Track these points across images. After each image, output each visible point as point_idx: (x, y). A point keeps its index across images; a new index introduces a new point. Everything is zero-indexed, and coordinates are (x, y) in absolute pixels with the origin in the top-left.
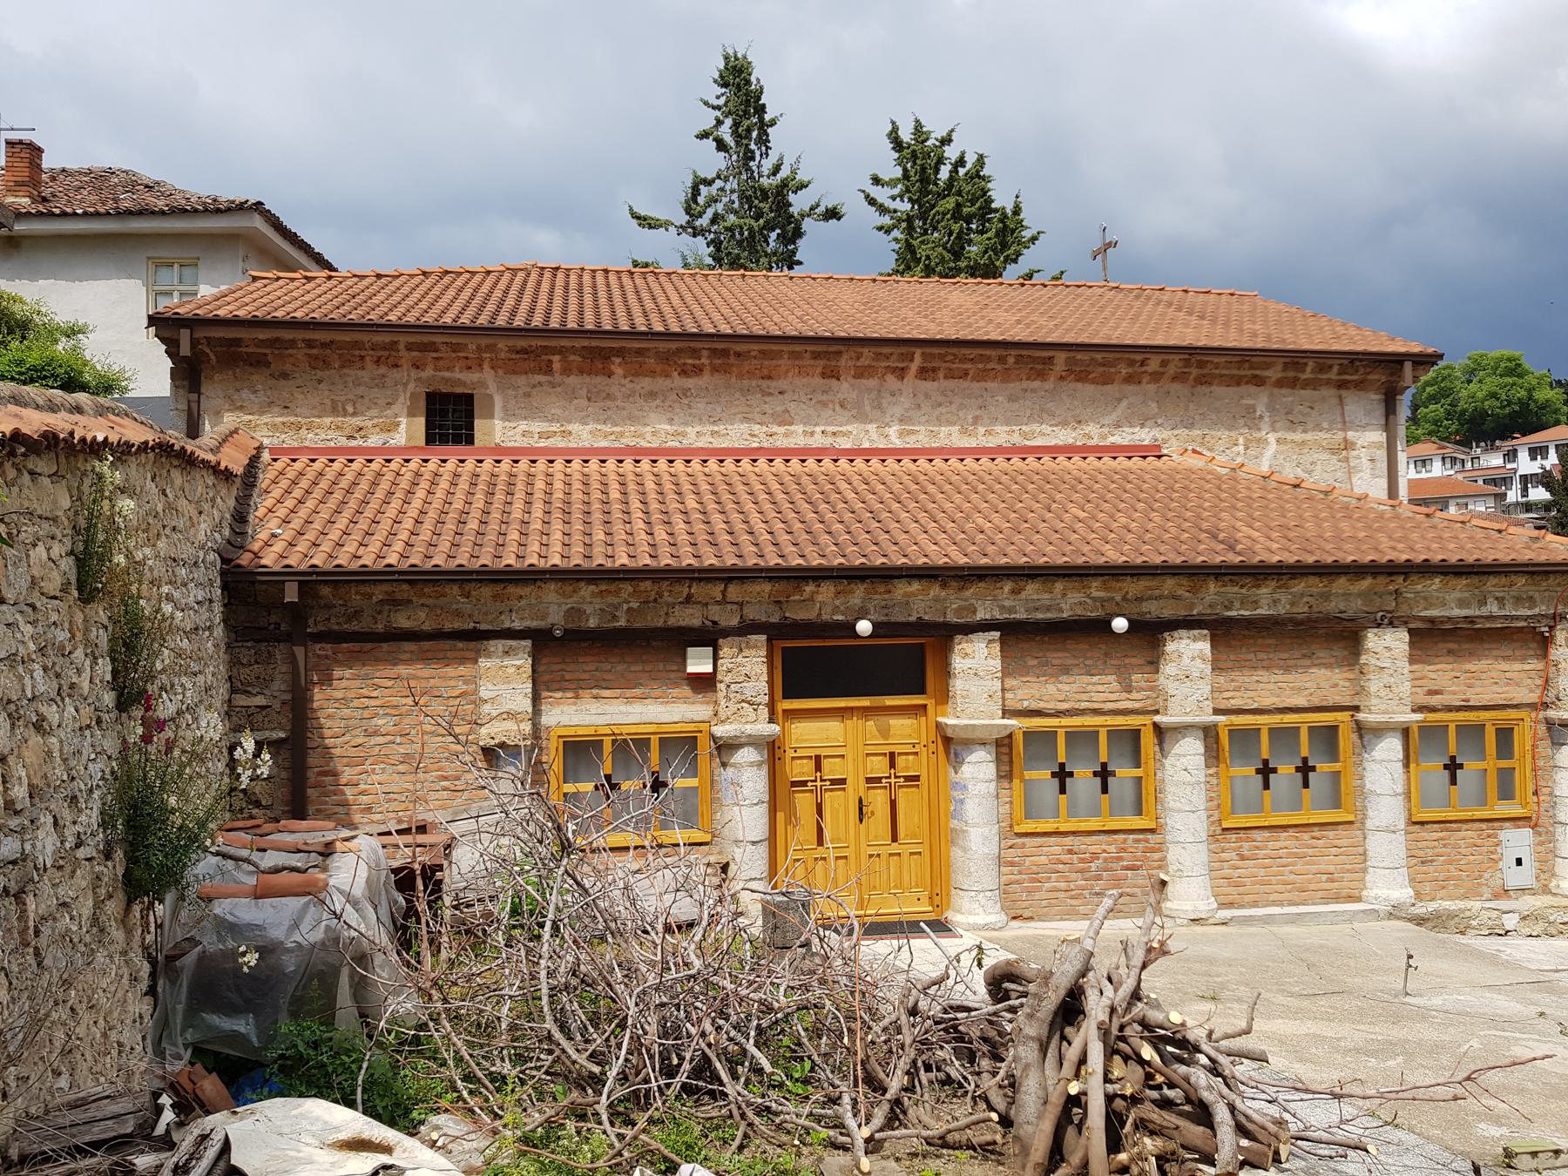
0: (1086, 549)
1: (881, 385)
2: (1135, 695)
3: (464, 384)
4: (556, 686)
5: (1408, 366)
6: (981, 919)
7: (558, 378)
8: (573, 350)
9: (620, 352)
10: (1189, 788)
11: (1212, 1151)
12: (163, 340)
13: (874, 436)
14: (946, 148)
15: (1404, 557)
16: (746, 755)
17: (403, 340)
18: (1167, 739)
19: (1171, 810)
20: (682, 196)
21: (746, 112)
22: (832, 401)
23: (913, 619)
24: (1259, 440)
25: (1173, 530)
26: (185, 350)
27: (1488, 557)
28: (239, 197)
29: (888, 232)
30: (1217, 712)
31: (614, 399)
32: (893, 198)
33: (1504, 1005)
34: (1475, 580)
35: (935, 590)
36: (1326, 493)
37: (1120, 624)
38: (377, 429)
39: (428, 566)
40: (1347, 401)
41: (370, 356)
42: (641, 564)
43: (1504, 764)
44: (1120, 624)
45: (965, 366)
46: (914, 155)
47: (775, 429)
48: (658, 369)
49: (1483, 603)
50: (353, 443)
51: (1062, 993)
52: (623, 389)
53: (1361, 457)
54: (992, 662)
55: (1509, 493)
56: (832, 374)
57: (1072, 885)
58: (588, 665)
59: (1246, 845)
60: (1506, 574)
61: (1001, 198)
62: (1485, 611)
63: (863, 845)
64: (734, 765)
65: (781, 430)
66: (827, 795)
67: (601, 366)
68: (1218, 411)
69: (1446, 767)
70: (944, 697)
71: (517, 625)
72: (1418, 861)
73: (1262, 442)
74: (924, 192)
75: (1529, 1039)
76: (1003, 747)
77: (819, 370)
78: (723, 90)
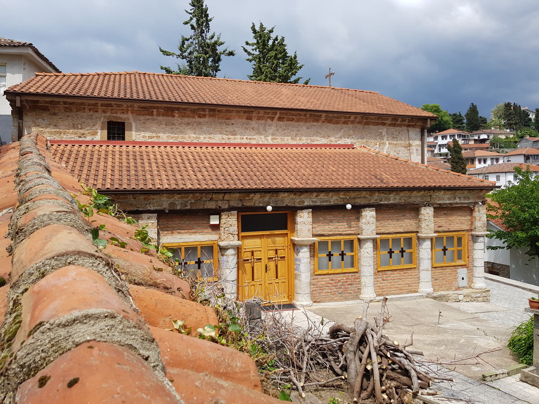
0: (338, 182)
2: (352, 229)
4: (165, 229)
5: (429, 120)
6: (305, 303)
7: (155, 117)
8: (161, 108)
9: (178, 109)
10: (368, 259)
11: (411, 385)
12: (9, 100)
13: (263, 140)
14: (271, 34)
15: (433, 185)
16: (231, 252)
17: (100, 103)
18: (362, 243)
19: (363, 266)
20: (179, 44)
21: (201, 16)
22: (250, 128)
23: (285, 205)
24: (383, 143)
25: (363, 175)
26: (18, 104)
27: (457, 185)
28: (23, 41)
29: (251, 61)
30: (377, 234)
31: (175, 125)
32: (253, 50)
33: (467, 326)
34: (453, 192)
35: (292, 196)
36: (406, 162)
37: (349, 206)
38: (90, 134)
39: (122, 189)
40: (410, 131)
41: (87, 108)
42: (196, 188)
43: (459, 248)
44: (349, 206)
45: (293, 117)
46: (260, 37)
47: (231, 137)
48: (191, 115)
49: (455, 199)
50: (81, 139)
51: (360, 336)
52: (178, 122)
53: (414, 149)
54: (309, 219)
55: (435, 150)
56: (250, 118)
57: (332, 291)
58: (176, 222)
59: (384, 276)
60: (462, 190)
61: (290, 53)
62: (455, 201)
63: (267, 280)
64: (226, 255)
65: (233, 137)
66: (255, 264)
67: (170, 113)
68: (371, 133)
69: (443, 250)
70: (293, 230)
71: (152, 208)
72: (434, 279)
73: (384, 144)
74: (264, 49)
75: (477, 338)
76: (312, 247)
77: (245, 117)
78: (193, 7)
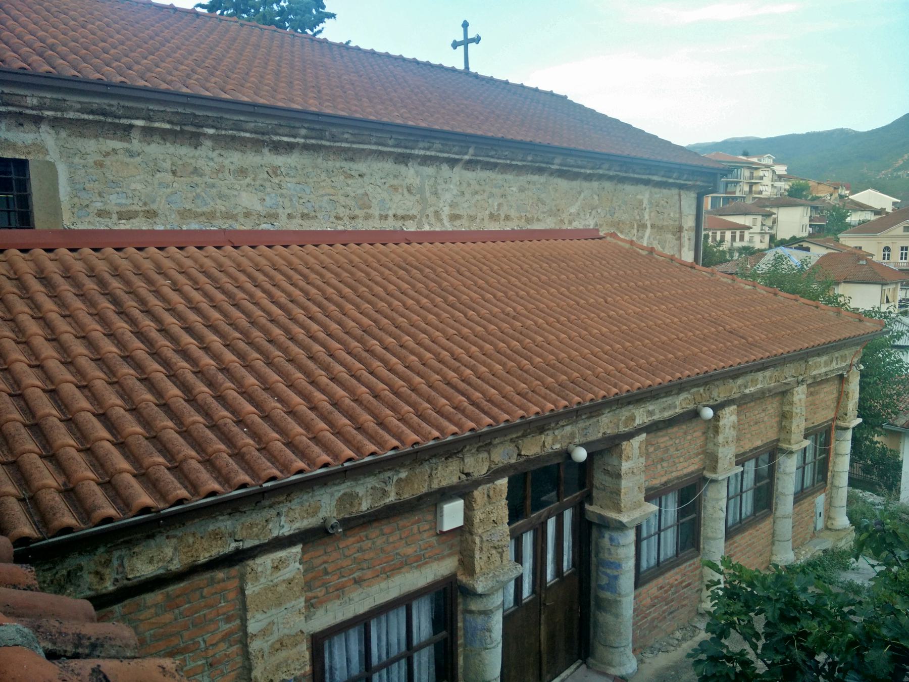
1: (438, 172)
3: (13, 146)
52: (211, 164)
71: (287, 530)
